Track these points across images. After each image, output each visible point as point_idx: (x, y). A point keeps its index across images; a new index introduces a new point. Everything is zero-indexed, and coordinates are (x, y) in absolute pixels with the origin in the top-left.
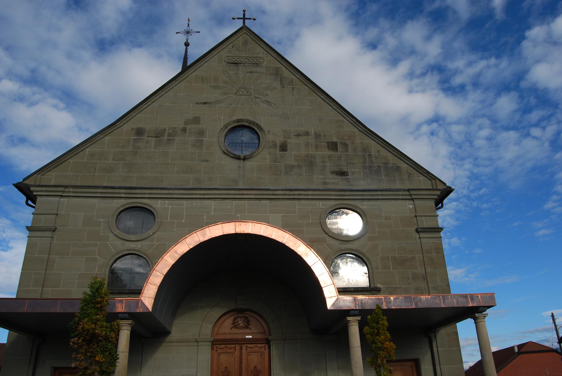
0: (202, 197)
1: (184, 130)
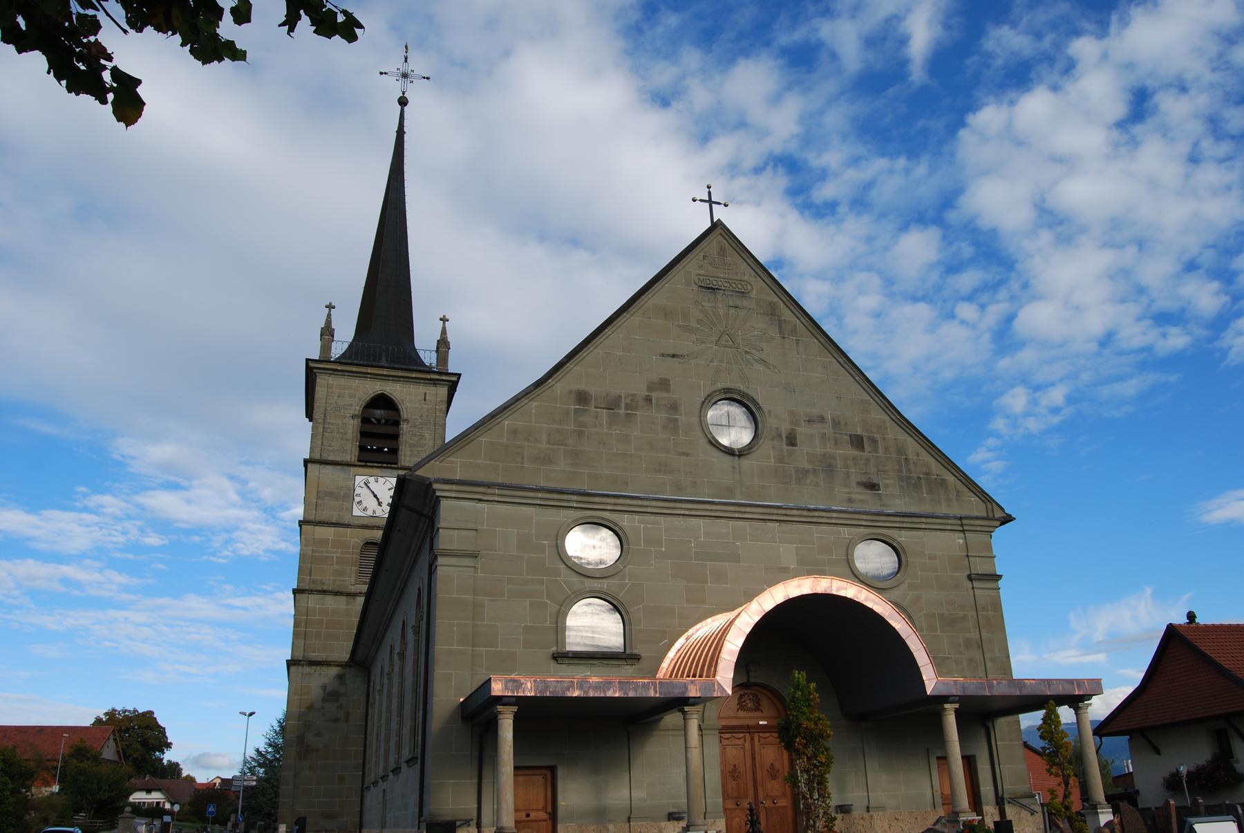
1: (648, 400)
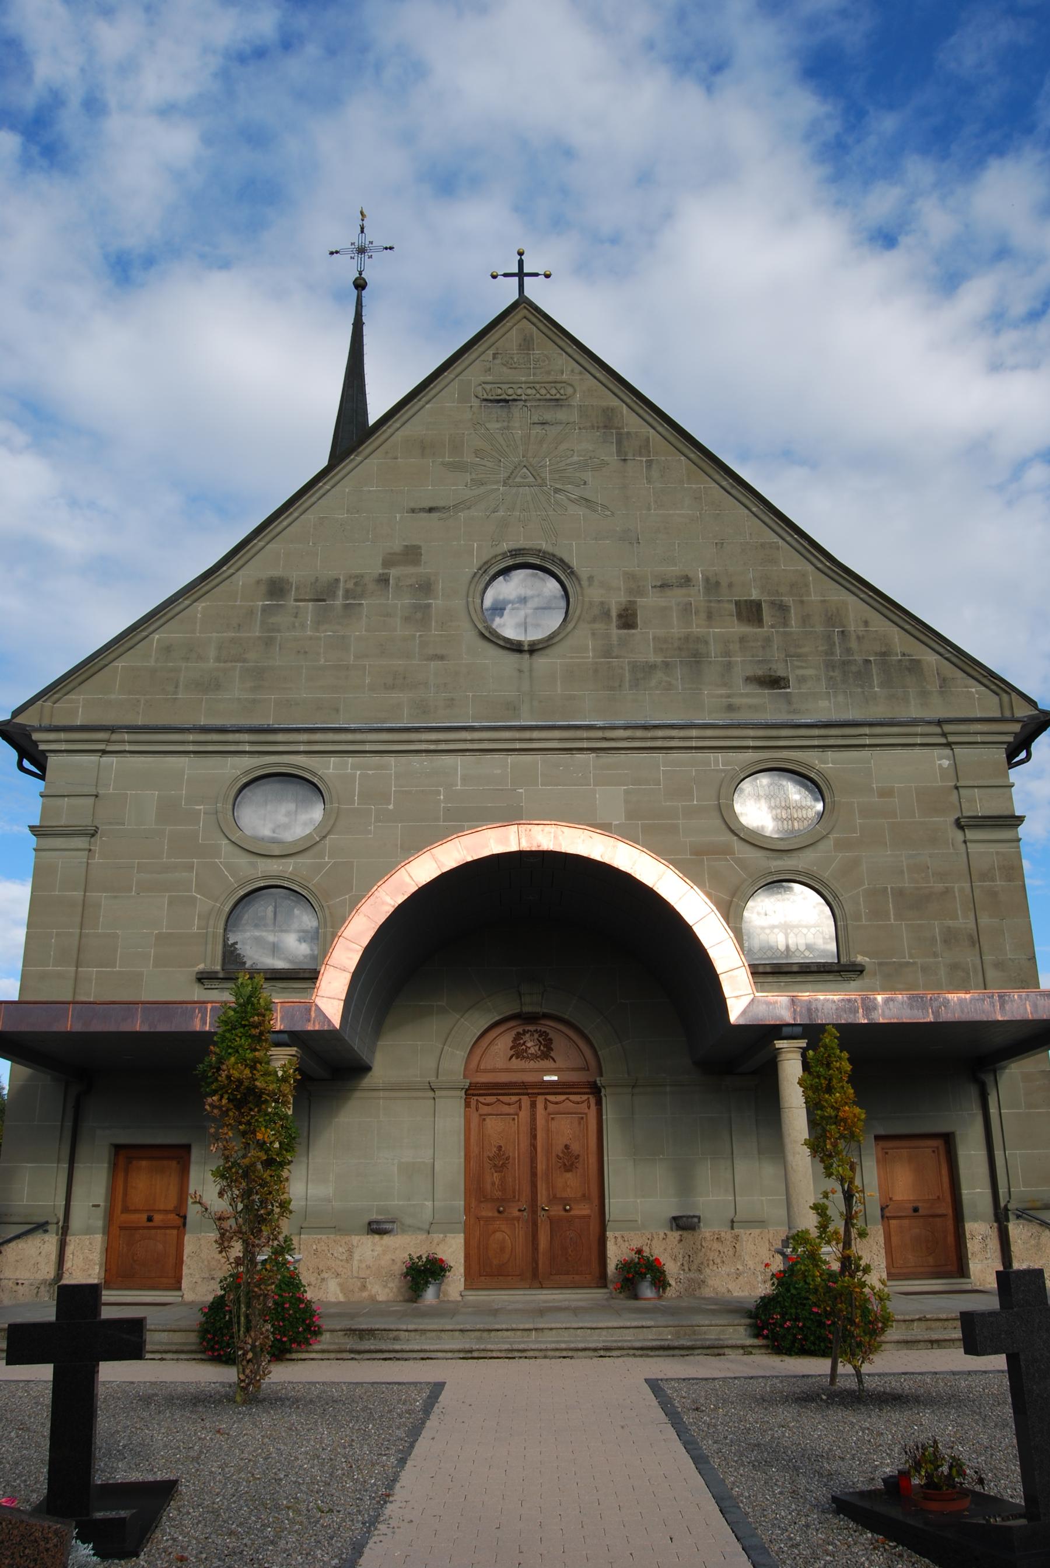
0: (432, 747)
1: (383, 580)
